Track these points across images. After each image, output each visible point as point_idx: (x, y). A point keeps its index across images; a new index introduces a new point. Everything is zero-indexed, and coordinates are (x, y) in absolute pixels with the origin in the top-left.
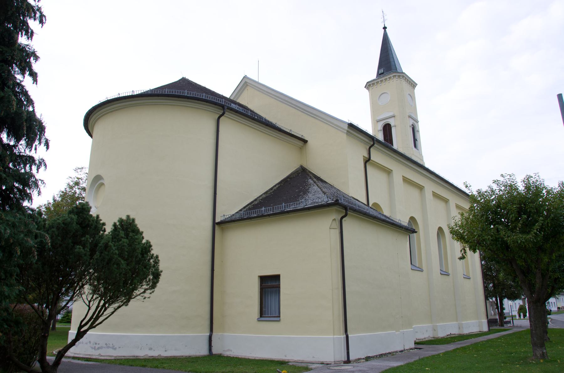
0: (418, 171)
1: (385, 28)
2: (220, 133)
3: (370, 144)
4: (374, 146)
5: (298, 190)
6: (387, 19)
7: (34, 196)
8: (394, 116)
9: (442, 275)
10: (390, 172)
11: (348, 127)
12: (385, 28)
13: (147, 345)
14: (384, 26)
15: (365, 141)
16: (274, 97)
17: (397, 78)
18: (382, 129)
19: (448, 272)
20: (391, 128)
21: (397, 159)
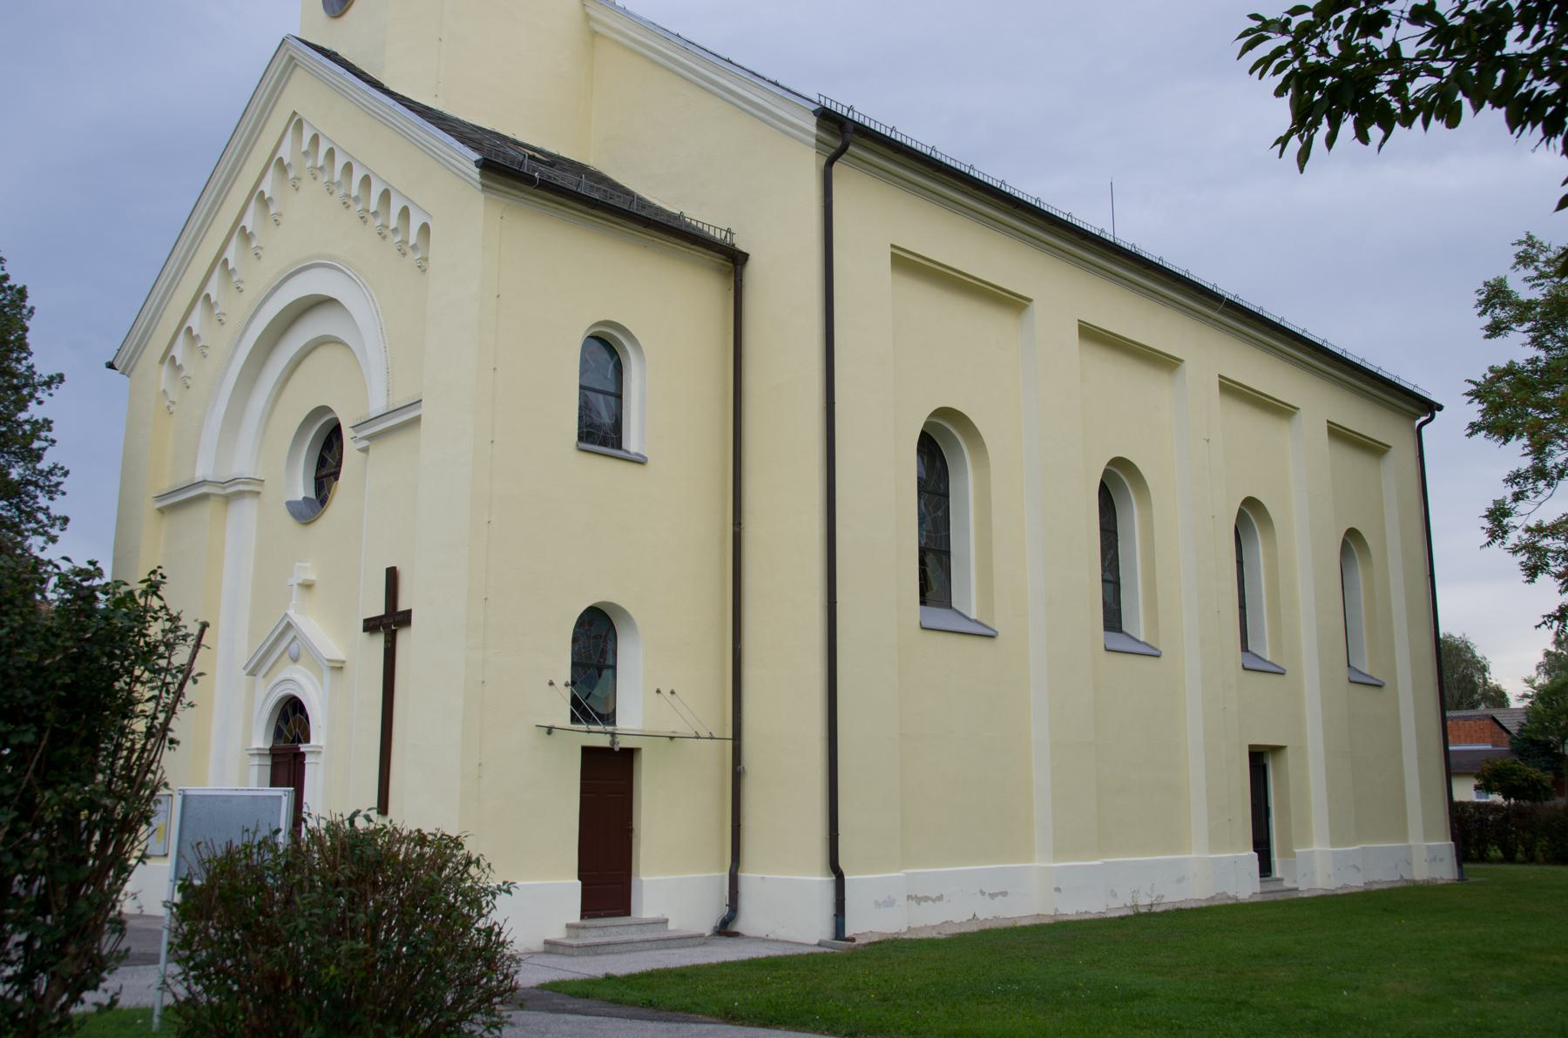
0: (1279, 350)
2: (272, 147)
3: (833, 148)
4: (848, 151)
9: (1353, 685)
11: (819, 126)
13: (1058, 890)
19: (1154, 645)
21: (1118, 276)
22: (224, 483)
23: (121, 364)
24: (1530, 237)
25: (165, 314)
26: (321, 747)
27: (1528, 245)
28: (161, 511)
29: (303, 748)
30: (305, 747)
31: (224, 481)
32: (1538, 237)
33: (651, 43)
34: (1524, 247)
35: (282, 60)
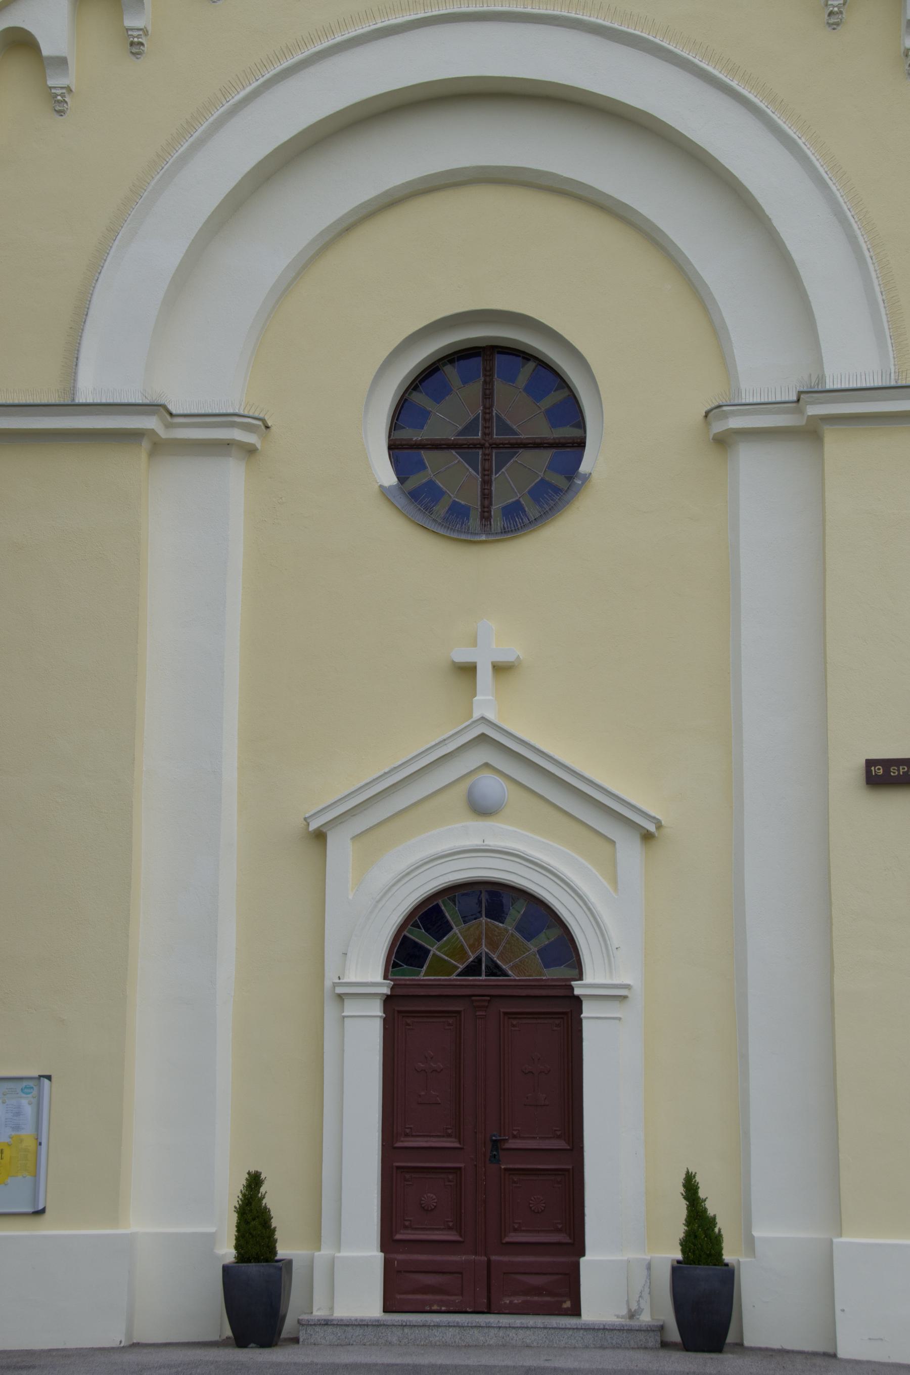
26: (627, 987)
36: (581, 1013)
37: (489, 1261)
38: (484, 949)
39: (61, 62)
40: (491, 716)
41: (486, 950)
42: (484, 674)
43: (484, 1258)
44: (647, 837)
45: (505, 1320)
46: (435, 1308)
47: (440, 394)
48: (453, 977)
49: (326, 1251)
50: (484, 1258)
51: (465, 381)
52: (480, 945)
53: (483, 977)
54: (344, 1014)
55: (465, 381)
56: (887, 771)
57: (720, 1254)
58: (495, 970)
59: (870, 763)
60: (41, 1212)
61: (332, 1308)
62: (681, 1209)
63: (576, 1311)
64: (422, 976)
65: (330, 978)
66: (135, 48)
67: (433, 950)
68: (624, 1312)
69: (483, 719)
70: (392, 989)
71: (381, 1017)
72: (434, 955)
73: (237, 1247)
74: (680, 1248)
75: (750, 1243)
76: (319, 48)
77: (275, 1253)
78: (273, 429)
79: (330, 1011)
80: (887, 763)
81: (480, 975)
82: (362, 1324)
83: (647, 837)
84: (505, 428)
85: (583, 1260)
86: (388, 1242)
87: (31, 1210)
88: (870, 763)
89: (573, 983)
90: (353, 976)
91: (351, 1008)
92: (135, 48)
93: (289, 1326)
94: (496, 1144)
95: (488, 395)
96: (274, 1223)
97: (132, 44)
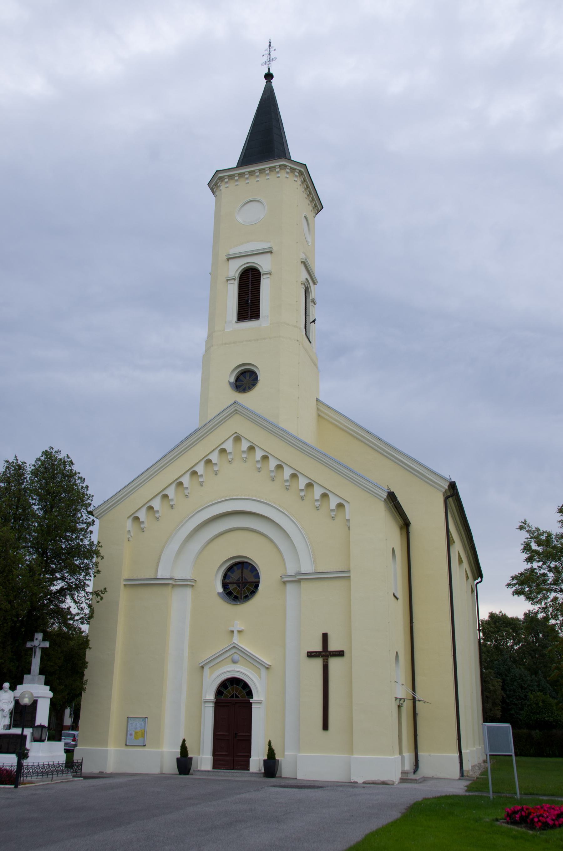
1: (269, 76)
5: (54, 588)
6: (275, 59)
7: (34, 657)
8: (271, 252)
10: (244, 683)
12: (269, 76)
14: (267, 72)
15: (472, 567)
16: (233, 414)
17: (287, 173)
18: (237, 276)
20: (260, 277)
22: (176, 580)
23: (96, 513)
24: (525, 521)
25: (131, 496)
26: (262, 701)
27: (524, 524)
28: (125, 585)
29: (251, 701)
30: (252, 700)
31: (176, 579)
32: (528, 522)
33: (354, 429)
34: (523, 524)
35: (232, 409)
36: (252, 706)
37: (233, 759)
38: (235, 692)
39: (158, 511)
40: (236, 642)
41: (552, 675)
42: (235, 633)
43: (233, 758)
44: (267, 668)
45: (235, 771)
46: (223, 768)
47: (233, 572)
48: (229, 698)
49: (201, 756)
50: (233, 758)
51: (238, 569)
52: (234, 691)
53: (234, 698)
54: (206, 706)
55: (238, 569)
56: (311, 654)
57: (275, 758)
58: (237, 696)
59: (308, 652)
60: (145, 746)
61: (201, 767)
62: (267, 747)
63: (249, 770)
64: (222, 698)
65: (203, 698)
66: (172, 507)
67: (225, 692)
68: (258, 770)
69: (234, 643)
70: (216, 700)
71: (213, 706)
72: (225, 694)
73: (180, 754)
74: (267, 756)
75: (283, 755)
76: (206, 506)
77: (188, 756)
78: (197, 581)
79: (203, 704)
80: (311, 652)
81: (234, 697)
82: (208, 771)
83: (267, 668)
84: (245, 579)
85: (250, 759)
86: (214, 754)
87: (143, 745)
88: (308, 652)
89: (250, 700)
90: (207, 698)
91: (207, 705)
92: (172, 507)
93: (191, 771)
94: (236, 734)
95: (242, 572)
96: (188, 749)
97: (171, 507)
